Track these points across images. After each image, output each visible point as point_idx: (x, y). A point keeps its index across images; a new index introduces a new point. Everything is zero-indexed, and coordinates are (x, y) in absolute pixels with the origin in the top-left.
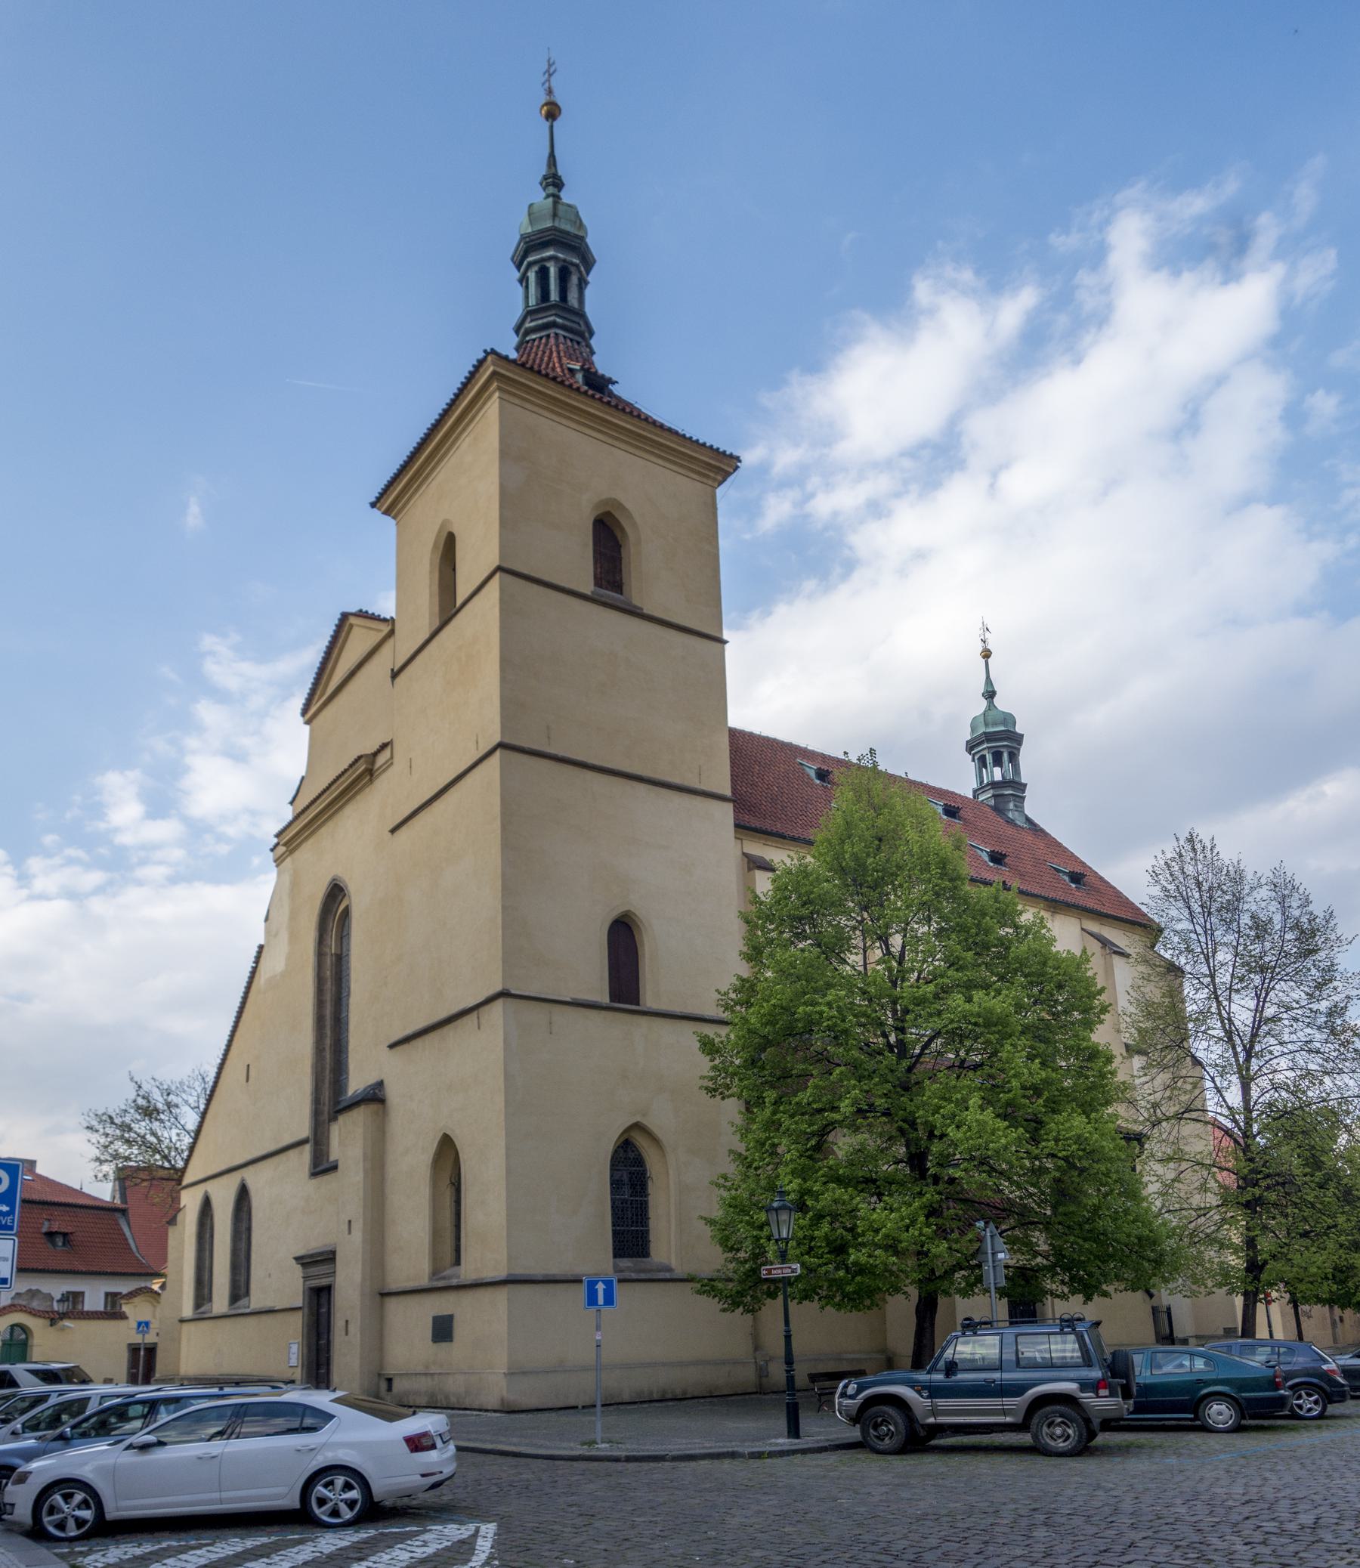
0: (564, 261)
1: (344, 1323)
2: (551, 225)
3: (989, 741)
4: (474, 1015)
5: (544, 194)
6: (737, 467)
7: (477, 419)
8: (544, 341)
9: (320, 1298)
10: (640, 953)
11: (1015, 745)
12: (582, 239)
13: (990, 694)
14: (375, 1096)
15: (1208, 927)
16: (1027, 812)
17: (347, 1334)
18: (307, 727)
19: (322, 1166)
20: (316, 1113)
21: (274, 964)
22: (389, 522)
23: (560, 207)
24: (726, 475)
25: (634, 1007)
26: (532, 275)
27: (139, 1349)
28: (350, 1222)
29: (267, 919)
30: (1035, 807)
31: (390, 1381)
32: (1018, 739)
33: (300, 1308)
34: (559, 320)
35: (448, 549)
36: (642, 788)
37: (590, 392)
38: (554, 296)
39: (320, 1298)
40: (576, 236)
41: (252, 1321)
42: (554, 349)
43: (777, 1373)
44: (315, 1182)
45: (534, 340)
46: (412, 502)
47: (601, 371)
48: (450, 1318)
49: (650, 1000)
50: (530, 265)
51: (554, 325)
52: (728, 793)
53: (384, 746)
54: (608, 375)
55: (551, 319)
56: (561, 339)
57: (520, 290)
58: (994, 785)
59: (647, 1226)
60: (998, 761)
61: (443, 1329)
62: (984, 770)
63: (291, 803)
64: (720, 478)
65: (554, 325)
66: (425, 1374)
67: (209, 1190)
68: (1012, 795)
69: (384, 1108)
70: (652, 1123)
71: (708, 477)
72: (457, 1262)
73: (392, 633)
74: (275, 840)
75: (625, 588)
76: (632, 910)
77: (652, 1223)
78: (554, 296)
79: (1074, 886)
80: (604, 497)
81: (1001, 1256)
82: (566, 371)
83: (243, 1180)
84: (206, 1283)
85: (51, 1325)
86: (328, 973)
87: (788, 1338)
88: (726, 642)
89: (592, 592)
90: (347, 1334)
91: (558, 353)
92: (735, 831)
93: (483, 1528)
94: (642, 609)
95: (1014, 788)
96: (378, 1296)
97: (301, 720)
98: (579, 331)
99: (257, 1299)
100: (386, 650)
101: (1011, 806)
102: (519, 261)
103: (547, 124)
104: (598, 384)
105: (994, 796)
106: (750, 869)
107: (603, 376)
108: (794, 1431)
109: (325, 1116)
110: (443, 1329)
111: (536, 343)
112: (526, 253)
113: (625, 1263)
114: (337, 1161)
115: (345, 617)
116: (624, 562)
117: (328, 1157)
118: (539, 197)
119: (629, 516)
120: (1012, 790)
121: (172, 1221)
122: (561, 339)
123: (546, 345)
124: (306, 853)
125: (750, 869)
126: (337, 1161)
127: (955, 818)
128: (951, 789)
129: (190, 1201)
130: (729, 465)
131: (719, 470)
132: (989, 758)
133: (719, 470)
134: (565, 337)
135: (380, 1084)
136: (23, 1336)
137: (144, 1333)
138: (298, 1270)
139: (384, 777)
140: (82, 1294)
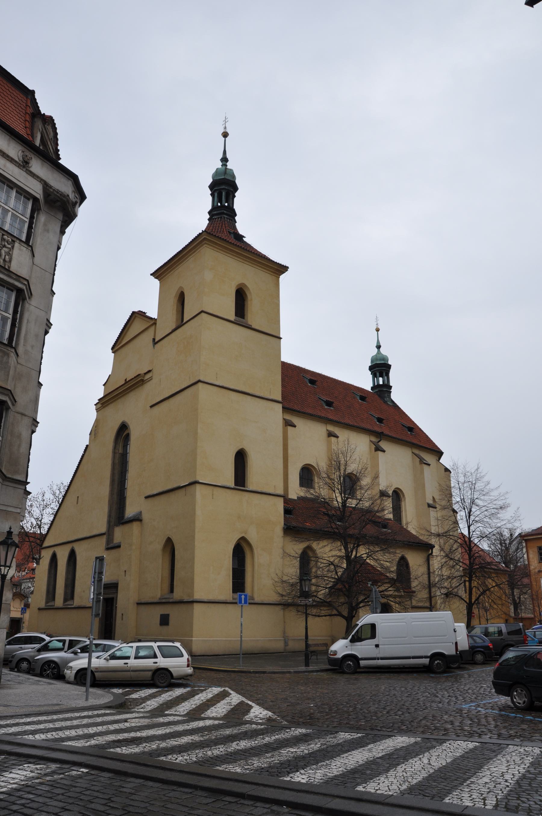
0: (228, 190)
1: (121, 615)
2: (223, 177)
3: (378, 367)
4: (183, 490)
6: (287, 270)
7: (197, 252)
8: (219, 219)
10: (246, 465)
12: (235, 182)
13: (379, 347)
17: (122, 620)
18: (113, 354)
19: (112, 547)
20: (109, 522)
22: (157, 282)
23: (227, 170)
26: (216, 194)
28: (125, 571)
30: (396, 396)
32: (389, 367)
35: (181, 298)
41: (75, 612)
42: (223, 223)
45: (216, 218)
46: (167, 276)
48: (168, 615)
49: (251, 487)
50: (216, 190)
51: (223, 213)
52: (280, 399)
53: (149, 371)
55: (222, 211)
58: (379, 385)
60: (381, 376)
62: (376, 379)
63: (104, 385)
65: (223, 213)
67: (56, 550)
68: (386, 391)
71: (276, 273)
72: (172, 590)
73: (155, 324)
75: (246, 317)
76: (244, 448)
77: (246, 579)
79: (409, 433)
82: (228, 233)
86: (117, 461)
88: (281, 338)
89: (235, 320)
90: (122, 620)
91: (225, 224)
92: (283, 412)
94: (252, 326)
96: (136, 605)
97: (111, 351)
98: (232, 214)
99: (77, 601)
101: (386, 395)
102: (211, 187)
103: (224, 139)
104: (240, 238)
105: (379, 391)
106: (286, 426)
107: (241, 235)
111: (217, 220)
114: (120, 542)
115: (133, 313)
118: (219, 165)
124: (110, 410)
125: (286, 426)
126: (120, 542)
127: (364, 401)
128: (363, 387)
129: (46, 556)
132: (378, 374)
134: (227, 218)
135: (141, 513)
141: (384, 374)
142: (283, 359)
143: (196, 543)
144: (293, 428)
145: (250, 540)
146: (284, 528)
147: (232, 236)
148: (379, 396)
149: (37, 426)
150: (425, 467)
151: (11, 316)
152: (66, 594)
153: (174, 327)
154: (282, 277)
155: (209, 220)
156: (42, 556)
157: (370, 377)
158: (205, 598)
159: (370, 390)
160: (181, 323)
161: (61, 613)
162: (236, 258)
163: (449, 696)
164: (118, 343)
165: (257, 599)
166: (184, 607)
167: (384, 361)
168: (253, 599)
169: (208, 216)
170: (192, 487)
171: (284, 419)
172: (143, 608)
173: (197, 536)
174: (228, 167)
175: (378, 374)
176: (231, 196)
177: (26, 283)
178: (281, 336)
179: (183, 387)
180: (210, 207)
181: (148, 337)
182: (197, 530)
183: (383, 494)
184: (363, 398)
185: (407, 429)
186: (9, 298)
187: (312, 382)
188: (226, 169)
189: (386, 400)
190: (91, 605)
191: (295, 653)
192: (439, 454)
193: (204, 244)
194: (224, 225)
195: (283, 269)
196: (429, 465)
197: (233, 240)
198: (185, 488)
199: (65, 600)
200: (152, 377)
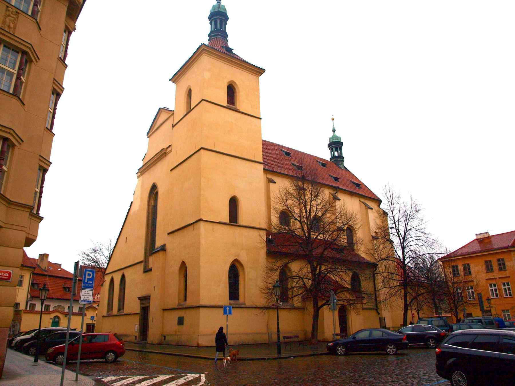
2: (217, 10)
5: (217, 2)
9: (145, 311)
11: (341, 145)
12: (226, 13)
13: (334, 131)
14: (163, 249)
15: (392, 203)
16: (344, 165)
19: (147, 270)
20: (146, 253)
21: (135, 208)
22: (174, 85)
24: (262, 74)
25: (236, 224)
27: (91, 325)
29: (134, 194)
31: (165, 337)
32: (342, 144)
33: (139, 313)
34: (219, 34)
35: (189, 93)
36: (239, 160)
37: (227, 53)
38: (218, 27)
39: (145, 311)
40: (224, 13)
41: (124, 317)
43: (275, 338)
44: (144, 274)
47: (230, 47)
48: (183, 317)
50: (213, 20)
51: (218, 35)
52: (262, 161)
53: (170, 146)
54: (232, 48)
56: (220, 39)
57: (210, 26)
59: (238, 291)
60: (336, 150)
61: (181, 321)
64: (260, 75)
65: (218, 35)
66: (176, 335)
67: (113, 275)
69: (165, 253)
70: (240, 259)
71: (257, 74)
72: (185, 300)
73: (173, 114)
74: (138, 171)
77: (240, 290)
78: (218, 27)
80: (230, 80)
81: (335, 301)
83: (123, 273)
84: (111, 305)
85: (66, 317)
87: (278, 324)
90: (153, 322)
91: (219, 42)
93: (202, 375)
95: (341, 158)
96: (162, 311)
99: (126, 310)
100: (171, 119)
101: (340, 163)
102: (210, 18)
104: (230, 50)
105: (335, 160)
106: (268, 182)
108: (279, 353)
109: (148, 254)
110: (181, 321)
112: (212, 17)
113: (232, 302)
114: (152, 268)
115: (160, 109)
116: (235, 97)
117: (148, 267)
119: (236, 85)
120: (341, 158)
121: (102, 285)
122: (220, 39)
123: (216, 40)
124: (146, 175)
125: (268, 182)
126: (152, 268)
127: (324, 167)
129: (108, 279)
130: (263, 71)
131: (260, 72)
132: (334, 149)
133: (260, 72)
134: (221, 38)
135: (165, 245)
136: (58, 320)
137: (92, 320)
138: (138, 301)
139: (169, 155)
140: (35, 304)
141: (338, 148)
142: (263, 139)
143: (201, 264)
144: (273, 184)
145: (241, 261)
146: (266, 252)
147: (224, 49)
148: (335, 164)
149: (49, 166)
150: (369, 211)
151: (16, 72)
152: (119, 305)
153: (185, 113)
154: (262, 78)
155: (209, 40)
156: (105, 280)
157: (329, 151)
158: (208, 303)
159: (329, 160)
160: (189, 110)
161: (117, 318)
162: (227, 63)
163: (392, 381)
164: (151, 130)
165: (248, 304)
166: (192, 311)
167: (337, 139)
168: (245, 304)
169: (208, 38)
170: (198, 223)
171: (267, 178)
172: (167, 313)
173: (202, 258)
174: (221, 4)
175: (334, 149)
176: (224, 24)
177: (30, 46)
178: (261, 118)
179: (191, 153)
180: (209, 31)
181: (169, 124)
182: (201, 254)
183: (340, 229)
184: (324, 165)
185: (355, 185)
186: (16, 58)
187: (288, 154)
188: (219, 5)
189: (340, 166)
190: (139, 312)
191: (273, 343)
192: (379, 202)
193: (203, 54)
194: (218, 42)
195: (259, 71)
196: (372, 209)
197: (224, 50)
198: (192, 225)
199: (119, 310)
200: (171, 150)
